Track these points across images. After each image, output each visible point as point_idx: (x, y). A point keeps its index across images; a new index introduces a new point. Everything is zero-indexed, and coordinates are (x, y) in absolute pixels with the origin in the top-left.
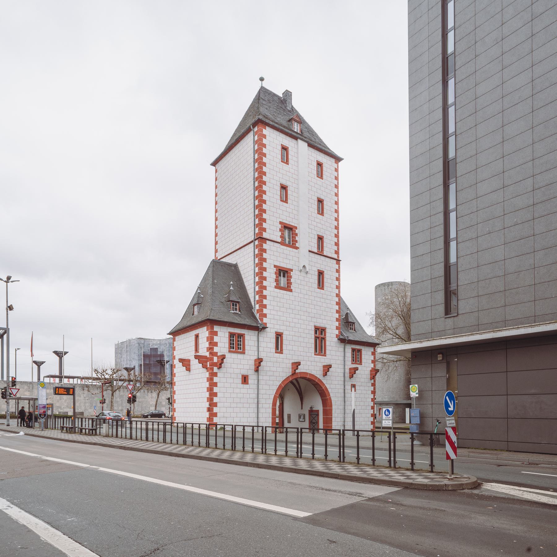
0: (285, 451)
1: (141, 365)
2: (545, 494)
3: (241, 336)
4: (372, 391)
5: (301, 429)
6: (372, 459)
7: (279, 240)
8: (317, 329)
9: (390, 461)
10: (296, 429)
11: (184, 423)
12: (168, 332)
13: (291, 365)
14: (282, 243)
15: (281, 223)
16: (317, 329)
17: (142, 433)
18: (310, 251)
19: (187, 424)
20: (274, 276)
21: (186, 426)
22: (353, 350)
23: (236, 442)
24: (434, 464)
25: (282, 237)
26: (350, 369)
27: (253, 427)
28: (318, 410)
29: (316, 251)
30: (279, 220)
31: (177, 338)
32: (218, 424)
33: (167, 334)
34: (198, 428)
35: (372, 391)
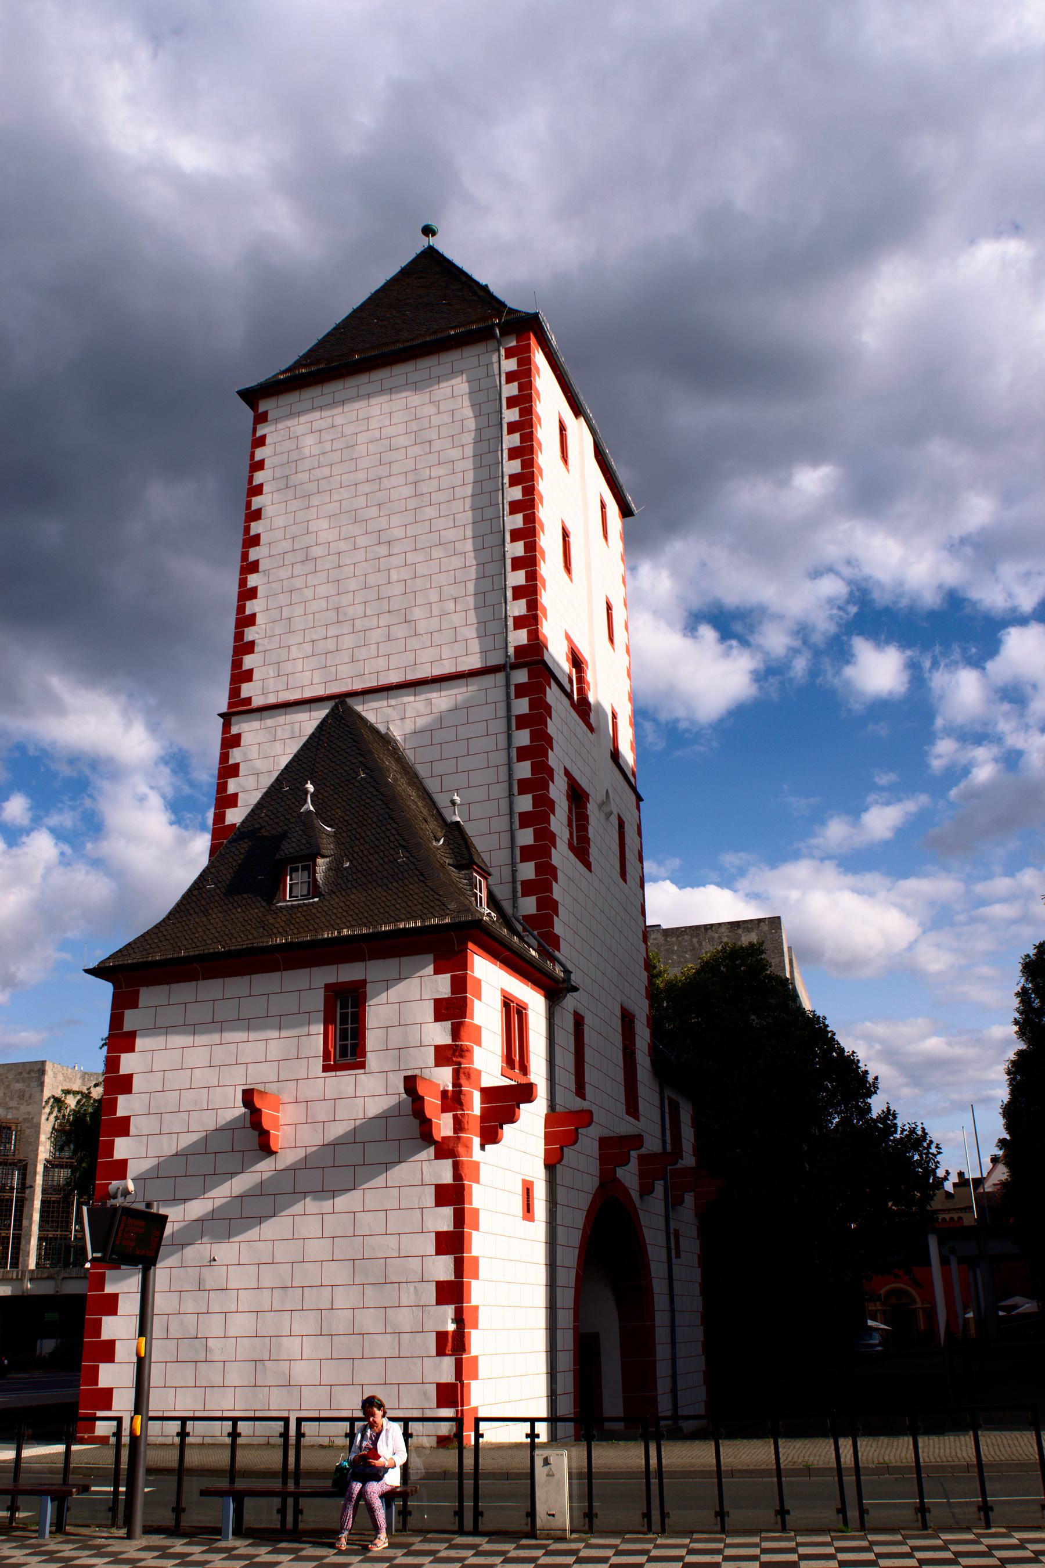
0: (173, 1510)
1: (627, 1019)
2: (700, 1554)
4: (477, 1278)
5: (300, 1421)
6: (457, 1509)
9: (459, 1513)
10: (282, 1423)
11: (286, 1420)
12: (91, 966)
13: (596, 1144)
17: (837, 1486)
19: (481, 1423)
21: (300, 1435)
23: (916, 1488)
24: (787, 1507)
27: (533, 1421)
28: (597, 1335)
31: (148, 996)
32: (480, 1415)
33: (87, 971)
34: (228, 1440)
35: (477, 1278)
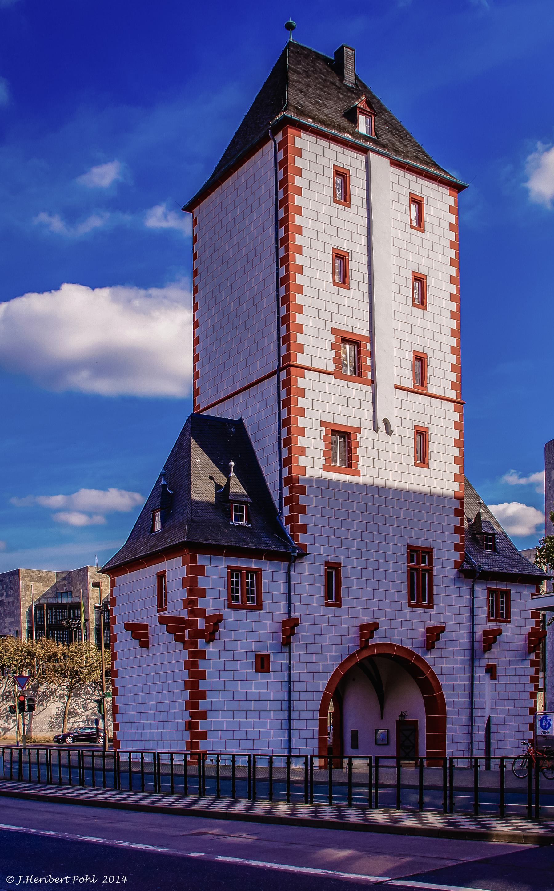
3: (256, 573)
7: (332, 367)
8: (413, 550)
14: (338, 374)
15: (334, 331)
16: (413, 550)
18: (397, 387)
20: (322, 445)
22: (491, 592)
25: (337, 360)
26: (485, 633)
29: (409, 384)
30: (330, 326)
